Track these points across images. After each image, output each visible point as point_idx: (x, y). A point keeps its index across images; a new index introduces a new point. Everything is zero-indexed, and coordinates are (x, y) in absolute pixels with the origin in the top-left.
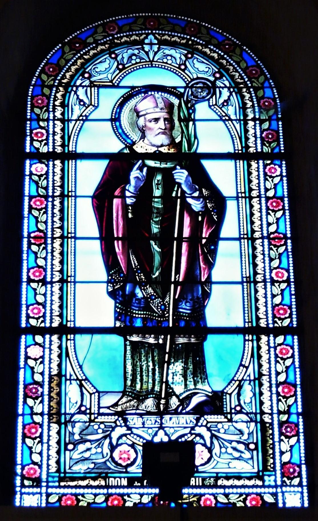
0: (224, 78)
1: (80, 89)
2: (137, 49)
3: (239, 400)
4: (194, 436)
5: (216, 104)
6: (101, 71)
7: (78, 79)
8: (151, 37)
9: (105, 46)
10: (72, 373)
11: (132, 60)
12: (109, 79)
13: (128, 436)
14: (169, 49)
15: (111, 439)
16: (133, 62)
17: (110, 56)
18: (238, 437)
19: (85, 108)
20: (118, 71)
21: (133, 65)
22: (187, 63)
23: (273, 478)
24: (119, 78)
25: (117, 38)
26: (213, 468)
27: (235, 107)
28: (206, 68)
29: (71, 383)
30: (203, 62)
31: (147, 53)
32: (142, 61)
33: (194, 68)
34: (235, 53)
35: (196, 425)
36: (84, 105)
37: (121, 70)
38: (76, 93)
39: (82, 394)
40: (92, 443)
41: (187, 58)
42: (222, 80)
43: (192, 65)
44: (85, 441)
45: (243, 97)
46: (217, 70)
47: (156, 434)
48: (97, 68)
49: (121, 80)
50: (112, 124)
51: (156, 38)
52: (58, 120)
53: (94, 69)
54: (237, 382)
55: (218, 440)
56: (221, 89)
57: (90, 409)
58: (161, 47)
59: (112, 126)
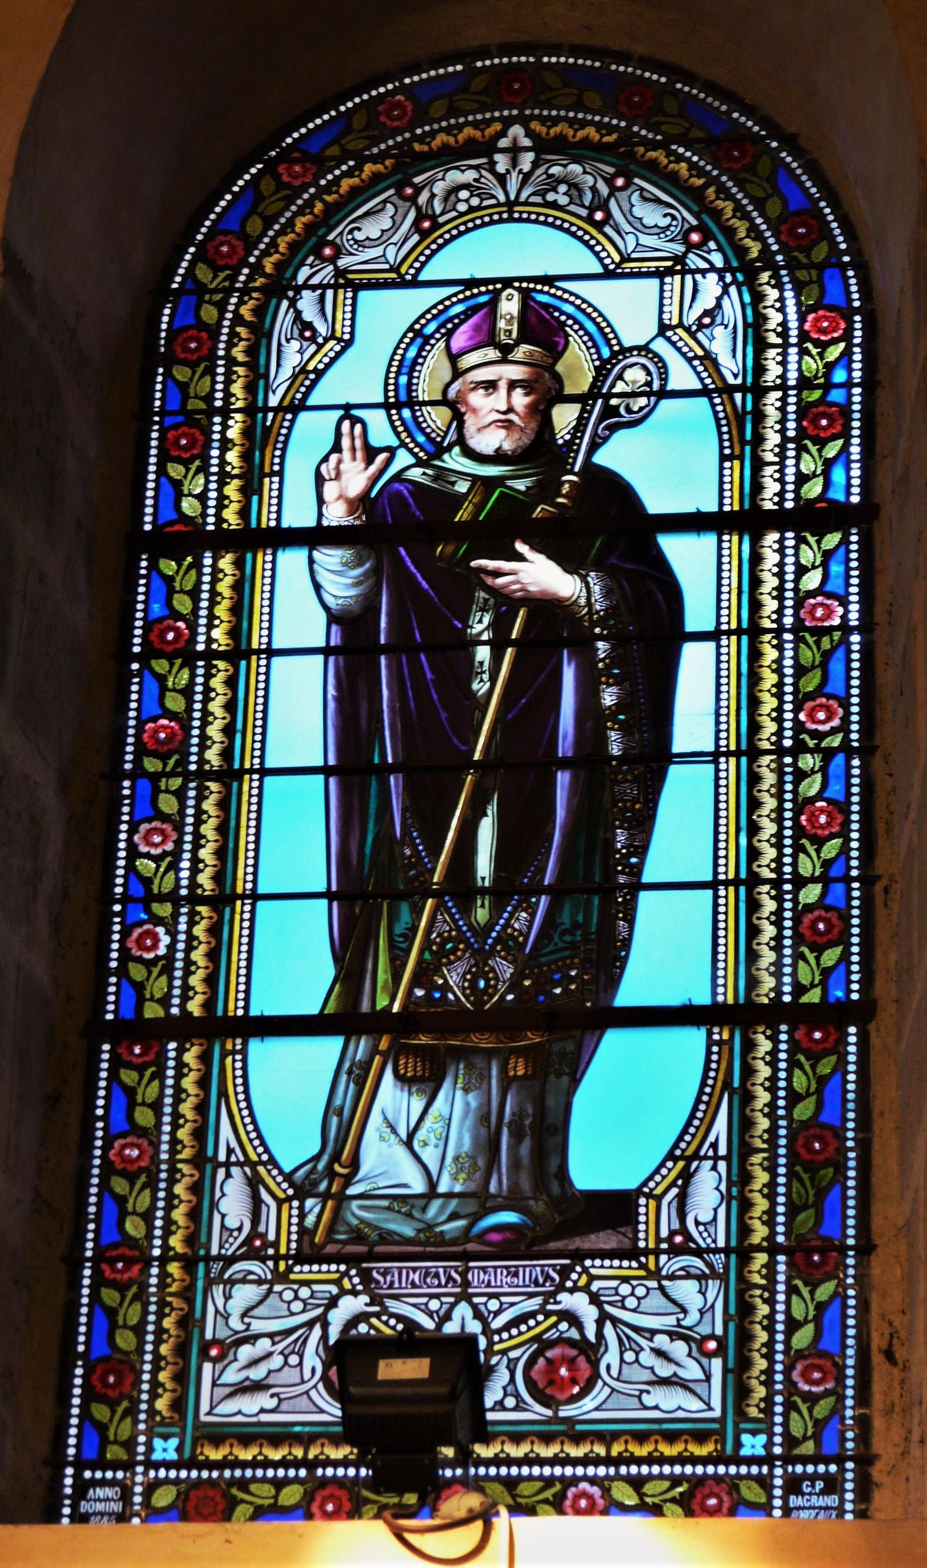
0: (712, 245)
1: (305, 293)
2: (477, 168)
3: (682, 1215)
4: (553, 1319)
5: (680, 325)
6: (368, 238)
7: (302, 264)
8: (517, 130)
9: (382, 163)
10: (234, 1144)
11: (459, 200)
12: (388, 262)
13: (374, 1321)
14: (565, 162)
15: (325, 1325)
16: (462, 207)
17: (400, 194)
18: (672, 1320)
19: (313, 348)
20: (416, 238)
21: (461, 214)
22: (613, 204)
23: (762, 1439)
24: (416, 260)
25: (421, 139)
26: (597, 1409)
27: (735, 327)
28: (665, 215)
29: (228, 1175)
30: (658, 201)
31: (502, 180)
32: (486, 203)
33: (630, 218)
34: (756, 174)
35: (561, 1288)
36: (313, 339)
37: (424, 234)
38: (293, 303)
39: (257, 1202)
40: (277, 1339)
41: (613, 190)
42: (705, 248)
43: (626, 207)
44: (253, 1339)
45: (758, 298)
46: (694, 222)
47: (448, 1317)
48: (359, 229)
49: (423, 264)
50: (389, 416)
51: (529, 134)
52: (178, 1257)
53: (351, 232)
54: (681, 1164)
55: (615, 1327)
56: (698, 277)
57: (276, 1245)
58: (543, 156)
59: (392, 422)
